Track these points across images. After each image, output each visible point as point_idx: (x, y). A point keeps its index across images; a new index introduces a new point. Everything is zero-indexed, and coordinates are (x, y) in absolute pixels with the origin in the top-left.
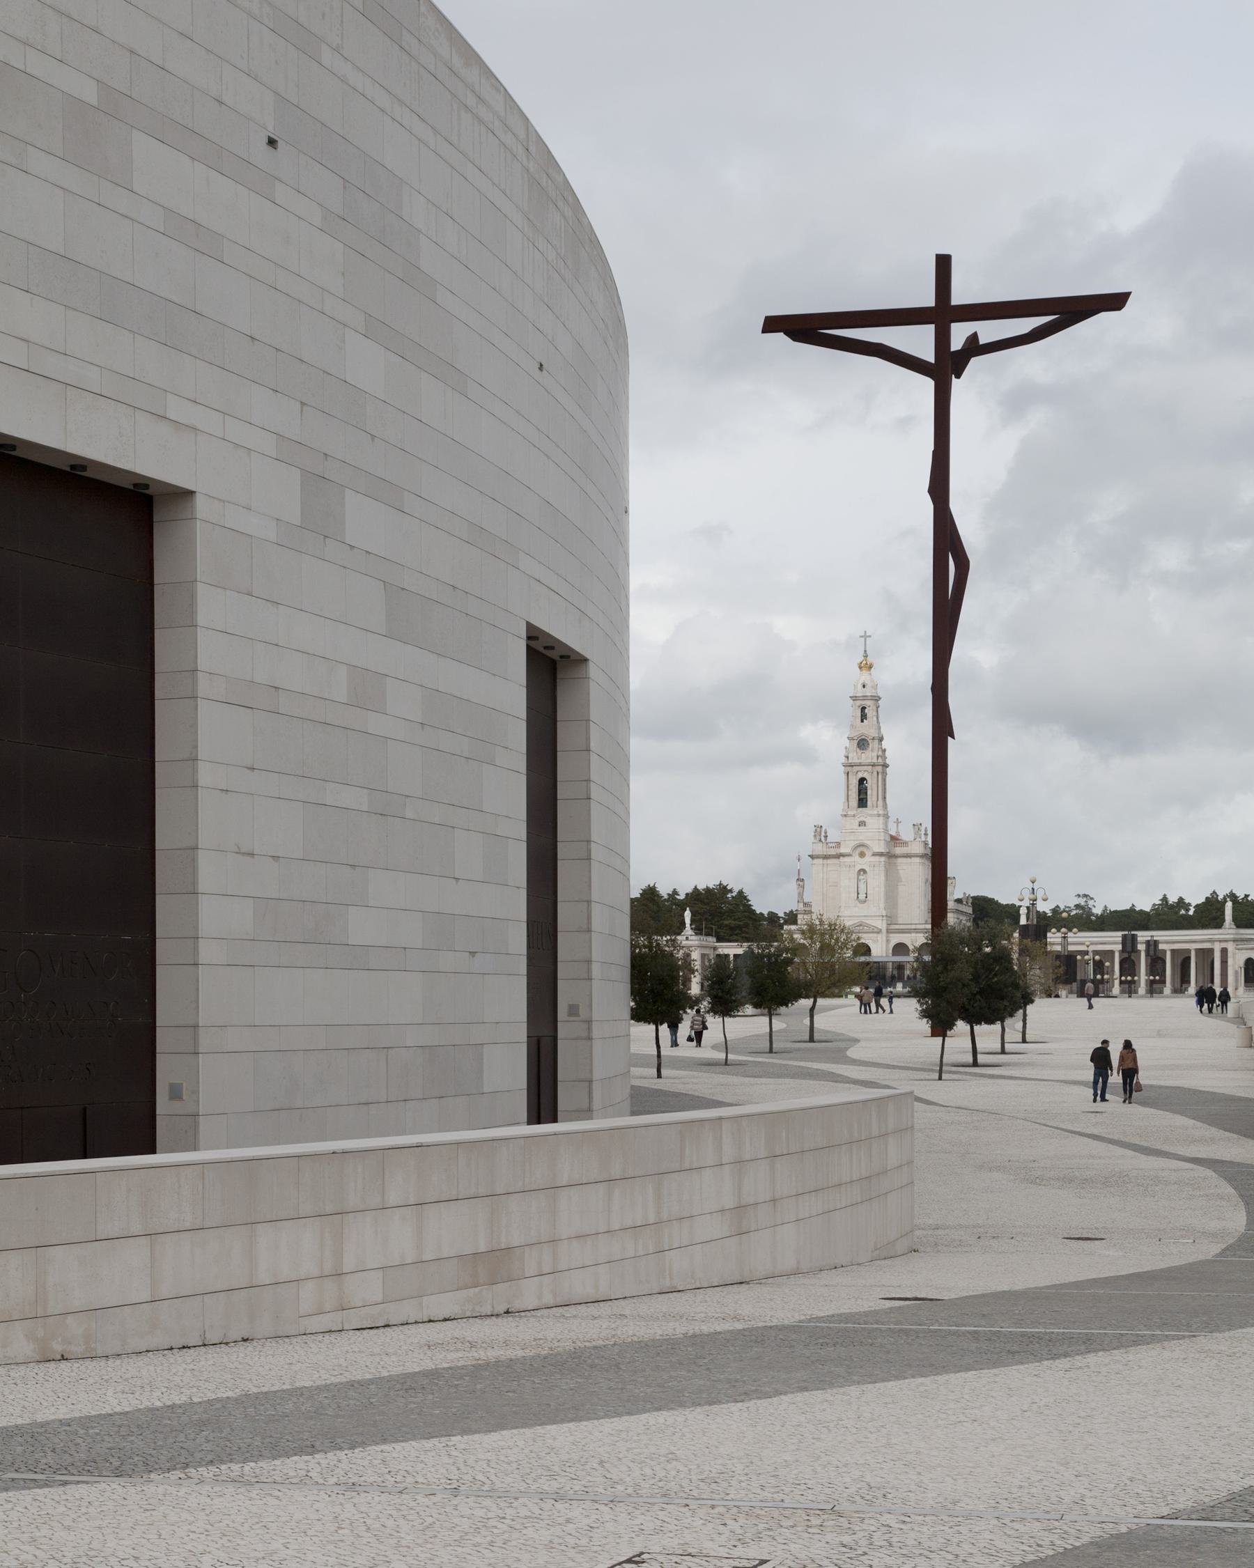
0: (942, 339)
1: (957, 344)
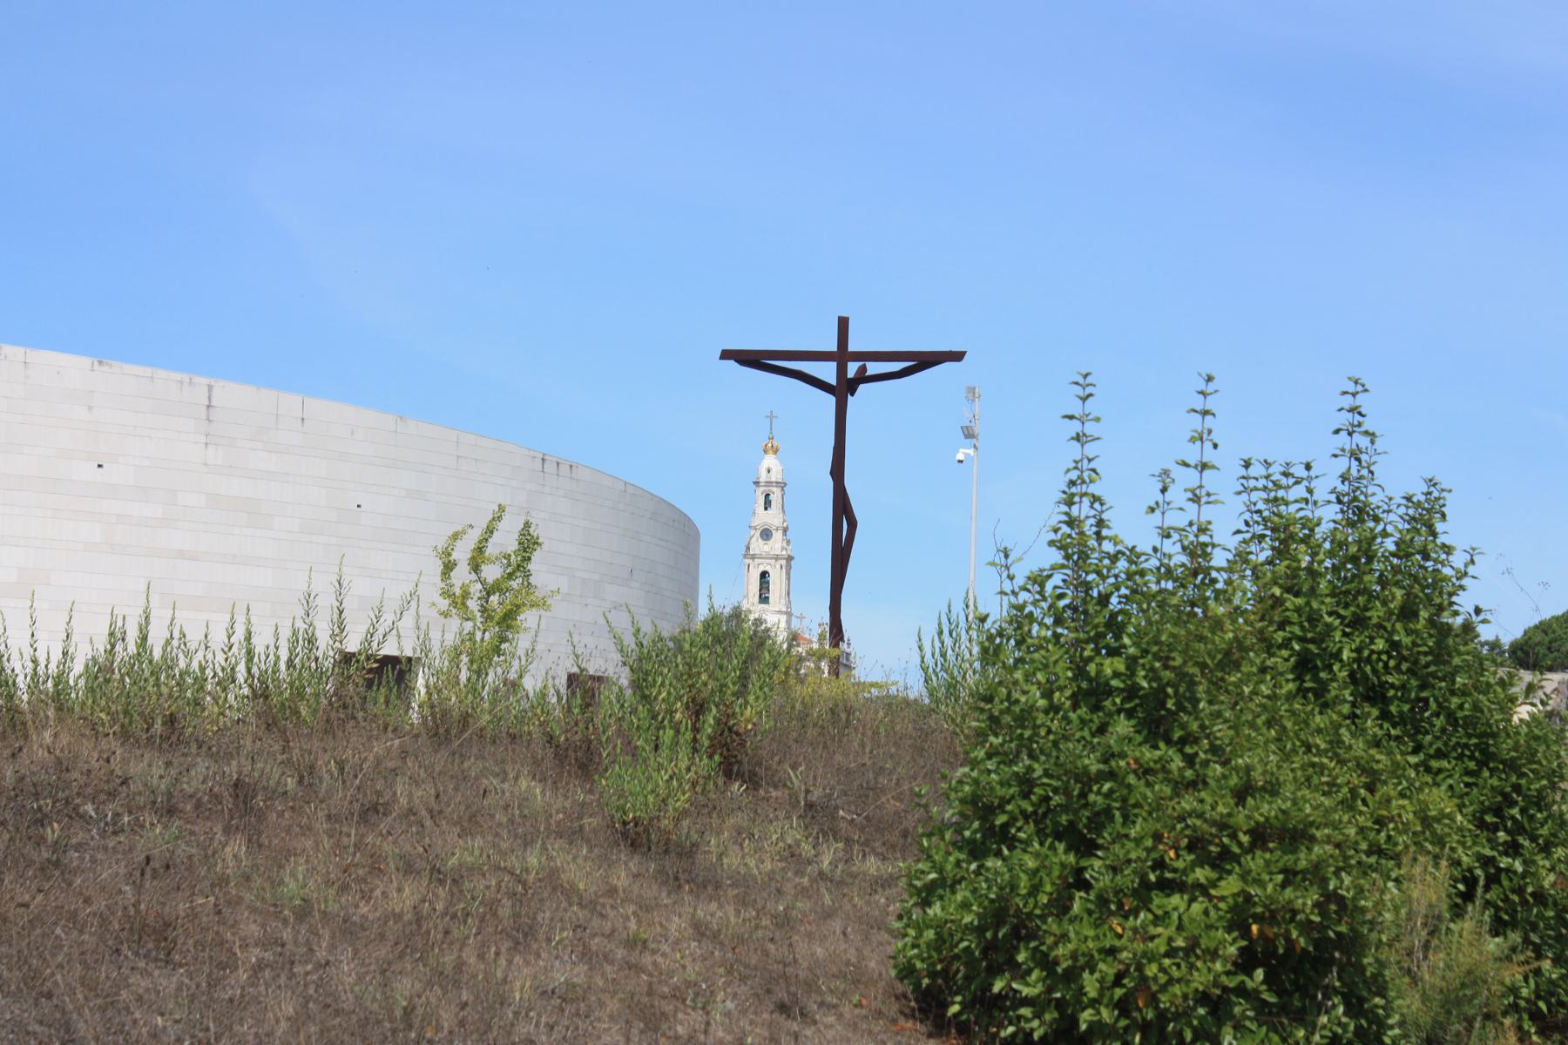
0: (842, 371)
1: (851, 373)
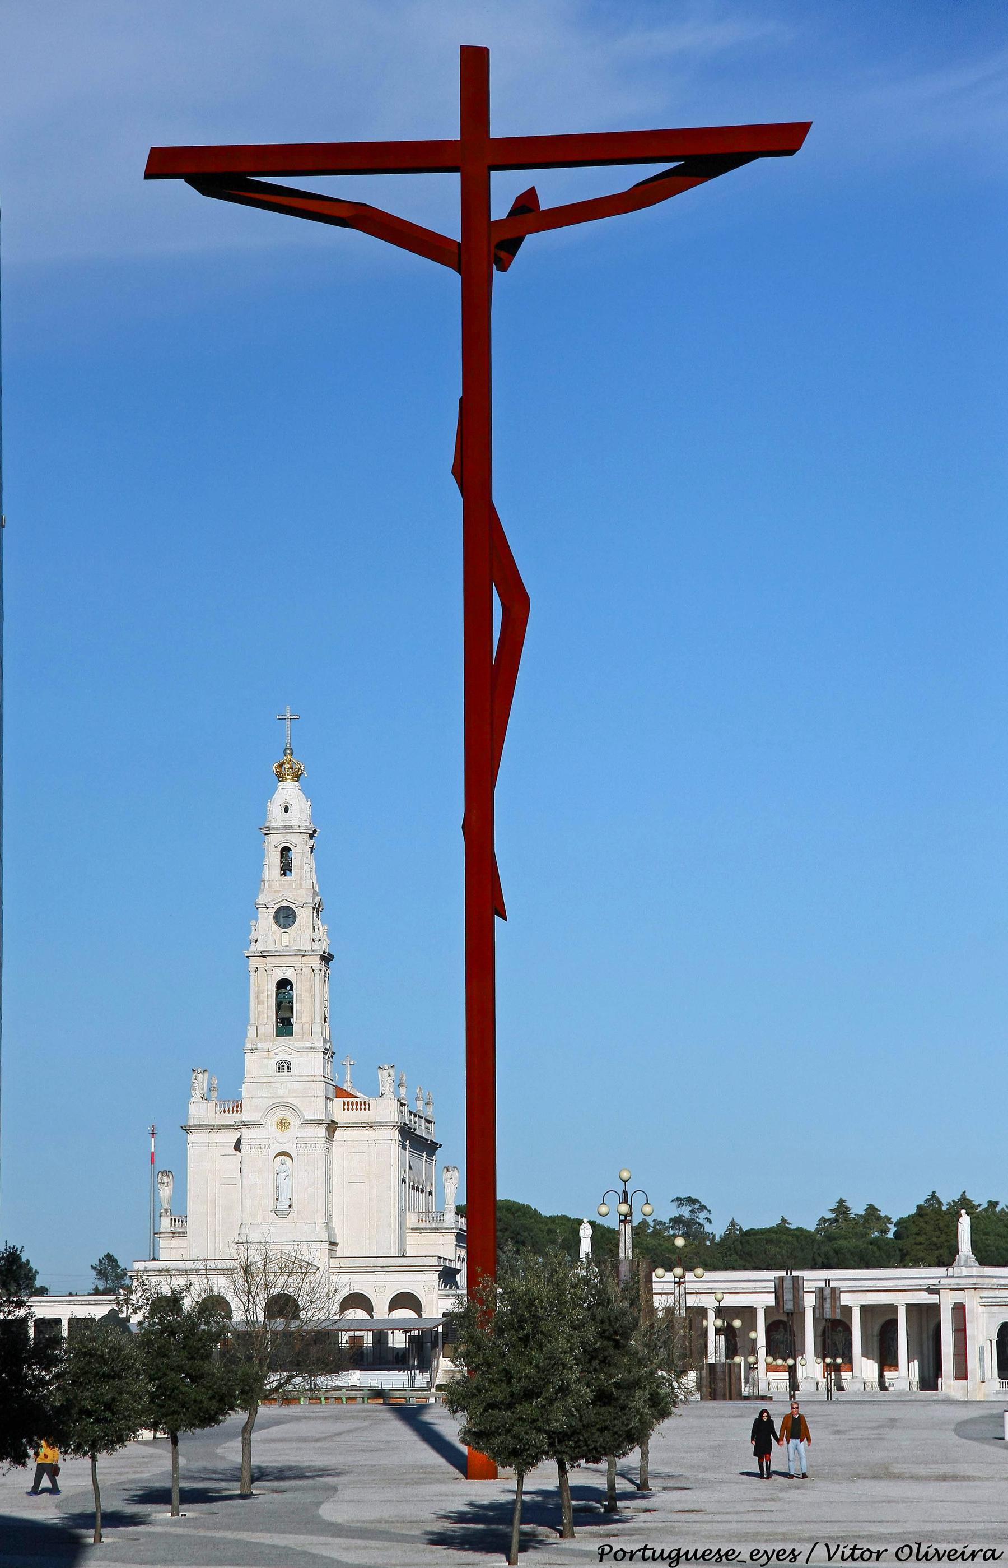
0: (475, 200)
1: (499, 209)
